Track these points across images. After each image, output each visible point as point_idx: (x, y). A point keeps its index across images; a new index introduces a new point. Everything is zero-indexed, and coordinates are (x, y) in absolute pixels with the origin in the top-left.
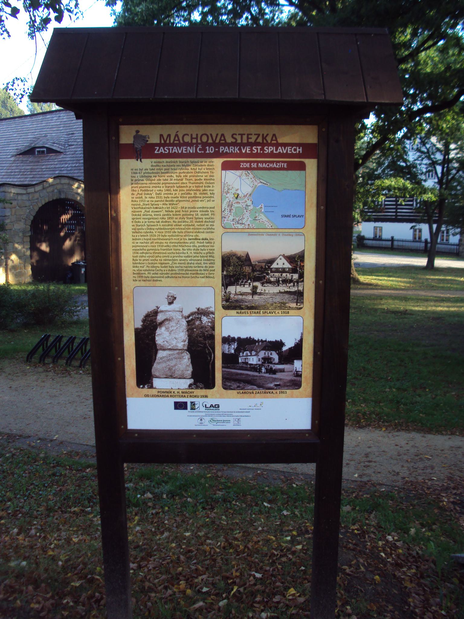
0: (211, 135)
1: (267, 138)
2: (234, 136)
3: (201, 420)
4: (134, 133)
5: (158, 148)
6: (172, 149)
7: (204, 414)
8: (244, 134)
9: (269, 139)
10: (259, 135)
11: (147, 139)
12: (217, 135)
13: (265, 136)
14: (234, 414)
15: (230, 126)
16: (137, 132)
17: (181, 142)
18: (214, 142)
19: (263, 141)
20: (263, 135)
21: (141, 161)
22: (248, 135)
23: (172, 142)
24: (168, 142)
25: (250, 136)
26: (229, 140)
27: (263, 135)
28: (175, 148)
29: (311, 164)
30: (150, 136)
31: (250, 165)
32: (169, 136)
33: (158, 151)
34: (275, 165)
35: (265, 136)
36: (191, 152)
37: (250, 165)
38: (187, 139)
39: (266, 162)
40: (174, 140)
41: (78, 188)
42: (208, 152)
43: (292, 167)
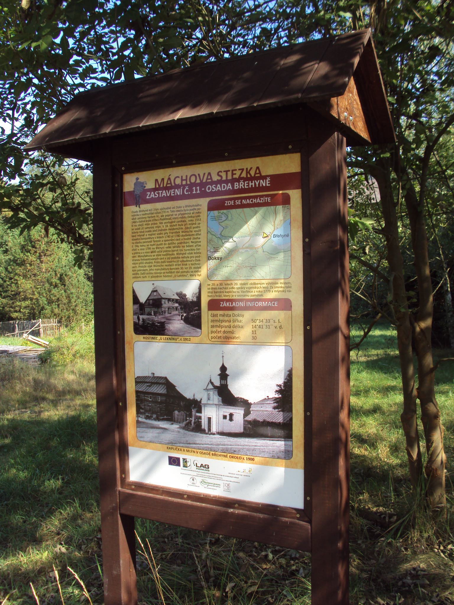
0: (199, 175)
1: (251, 172)
2: (220, 174)
3: (193, 480)
4: (135, 181)
5: (149, 193)
6: (162, 193)
7: (195, 474)
8: (229, 171)
9: (252, 173)
10: (243, 170)
11: (145, 185)
12: (204, 174)
13: (248, 170)
14: (224, 478)
15: (216, 163)
16: (137, 179)
17: (173, 184)
18: (201, 181)
19: (247, 175)
20: (247, 169)
21: (139, 207)
22: (233, 171)
23: (165, 186)
24: (162, 186)
25: (234, 172)
26: (215, 178)
27: (247, 169)
28: (164, 191)
29: (295, 195)
30: (148, 184)
31: (235, 203)
32: (163, 180)
33: (149, 196)
34: (258, 201)
35: (248, 170)
36: (179, 194)
37: (235, 203)
38: (178, 181)
39: (249, 198)
40: (167, 184)
41: (245, 44)
42: (194, 192)
43: (274, 202)
